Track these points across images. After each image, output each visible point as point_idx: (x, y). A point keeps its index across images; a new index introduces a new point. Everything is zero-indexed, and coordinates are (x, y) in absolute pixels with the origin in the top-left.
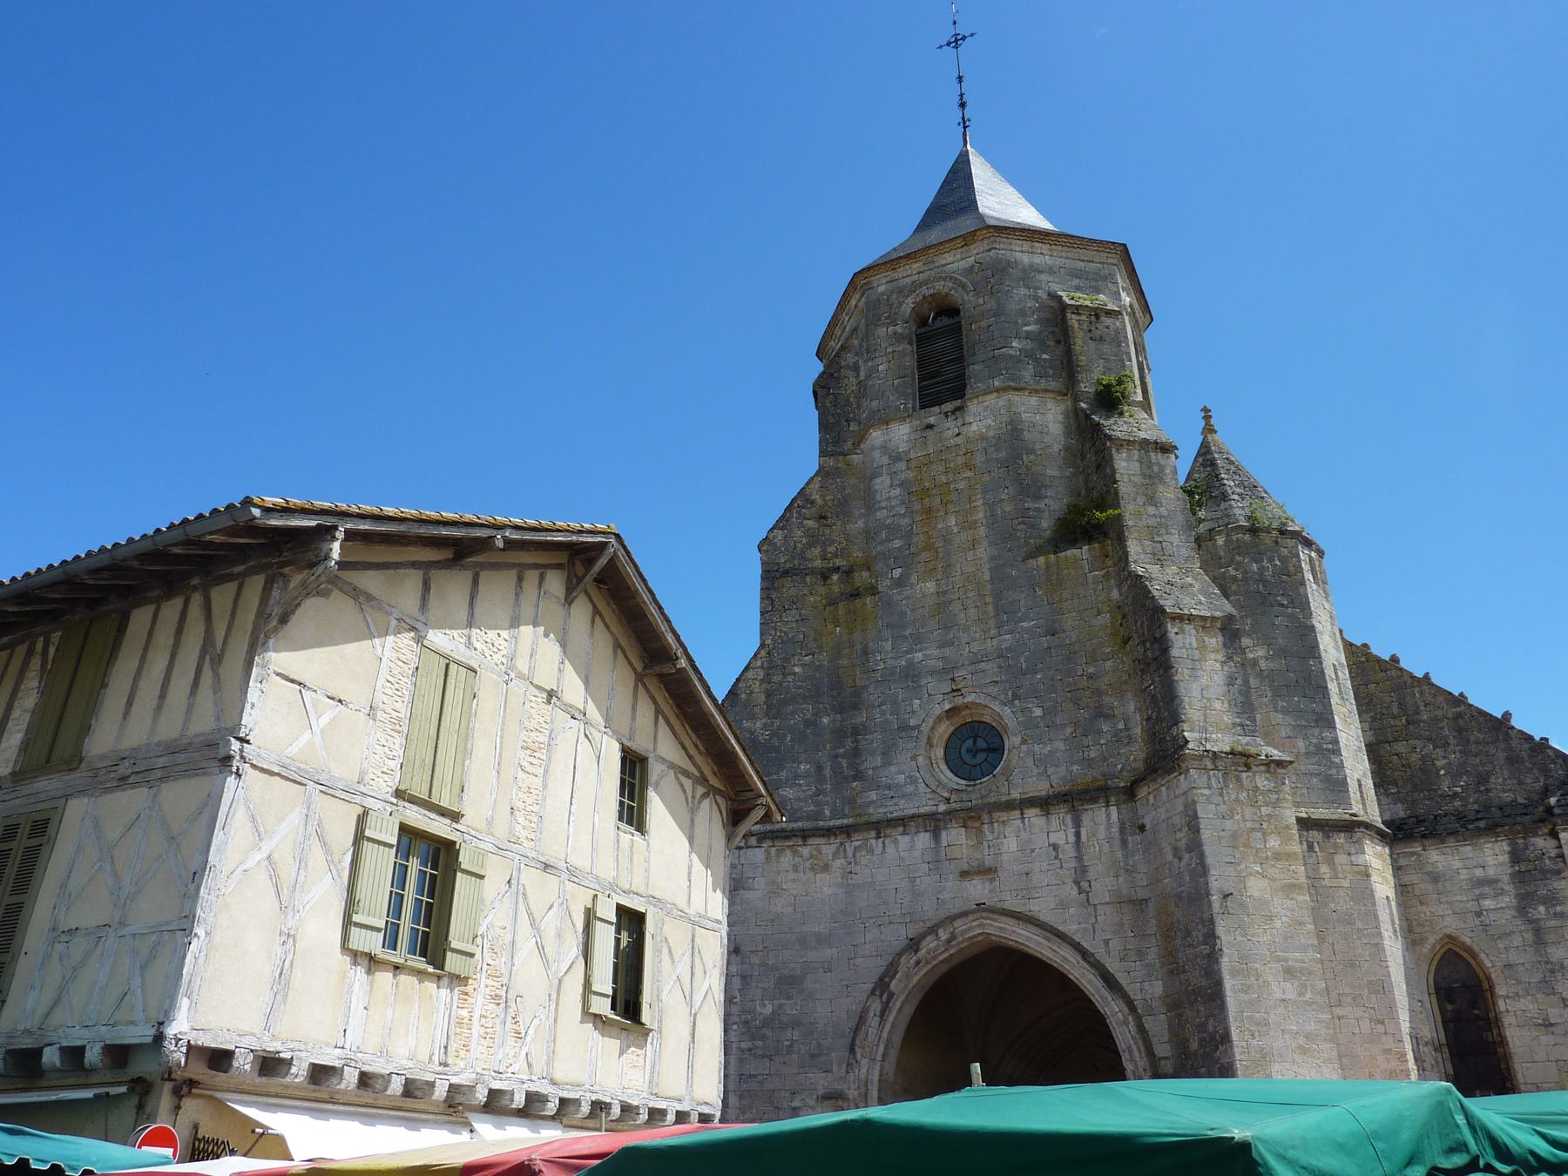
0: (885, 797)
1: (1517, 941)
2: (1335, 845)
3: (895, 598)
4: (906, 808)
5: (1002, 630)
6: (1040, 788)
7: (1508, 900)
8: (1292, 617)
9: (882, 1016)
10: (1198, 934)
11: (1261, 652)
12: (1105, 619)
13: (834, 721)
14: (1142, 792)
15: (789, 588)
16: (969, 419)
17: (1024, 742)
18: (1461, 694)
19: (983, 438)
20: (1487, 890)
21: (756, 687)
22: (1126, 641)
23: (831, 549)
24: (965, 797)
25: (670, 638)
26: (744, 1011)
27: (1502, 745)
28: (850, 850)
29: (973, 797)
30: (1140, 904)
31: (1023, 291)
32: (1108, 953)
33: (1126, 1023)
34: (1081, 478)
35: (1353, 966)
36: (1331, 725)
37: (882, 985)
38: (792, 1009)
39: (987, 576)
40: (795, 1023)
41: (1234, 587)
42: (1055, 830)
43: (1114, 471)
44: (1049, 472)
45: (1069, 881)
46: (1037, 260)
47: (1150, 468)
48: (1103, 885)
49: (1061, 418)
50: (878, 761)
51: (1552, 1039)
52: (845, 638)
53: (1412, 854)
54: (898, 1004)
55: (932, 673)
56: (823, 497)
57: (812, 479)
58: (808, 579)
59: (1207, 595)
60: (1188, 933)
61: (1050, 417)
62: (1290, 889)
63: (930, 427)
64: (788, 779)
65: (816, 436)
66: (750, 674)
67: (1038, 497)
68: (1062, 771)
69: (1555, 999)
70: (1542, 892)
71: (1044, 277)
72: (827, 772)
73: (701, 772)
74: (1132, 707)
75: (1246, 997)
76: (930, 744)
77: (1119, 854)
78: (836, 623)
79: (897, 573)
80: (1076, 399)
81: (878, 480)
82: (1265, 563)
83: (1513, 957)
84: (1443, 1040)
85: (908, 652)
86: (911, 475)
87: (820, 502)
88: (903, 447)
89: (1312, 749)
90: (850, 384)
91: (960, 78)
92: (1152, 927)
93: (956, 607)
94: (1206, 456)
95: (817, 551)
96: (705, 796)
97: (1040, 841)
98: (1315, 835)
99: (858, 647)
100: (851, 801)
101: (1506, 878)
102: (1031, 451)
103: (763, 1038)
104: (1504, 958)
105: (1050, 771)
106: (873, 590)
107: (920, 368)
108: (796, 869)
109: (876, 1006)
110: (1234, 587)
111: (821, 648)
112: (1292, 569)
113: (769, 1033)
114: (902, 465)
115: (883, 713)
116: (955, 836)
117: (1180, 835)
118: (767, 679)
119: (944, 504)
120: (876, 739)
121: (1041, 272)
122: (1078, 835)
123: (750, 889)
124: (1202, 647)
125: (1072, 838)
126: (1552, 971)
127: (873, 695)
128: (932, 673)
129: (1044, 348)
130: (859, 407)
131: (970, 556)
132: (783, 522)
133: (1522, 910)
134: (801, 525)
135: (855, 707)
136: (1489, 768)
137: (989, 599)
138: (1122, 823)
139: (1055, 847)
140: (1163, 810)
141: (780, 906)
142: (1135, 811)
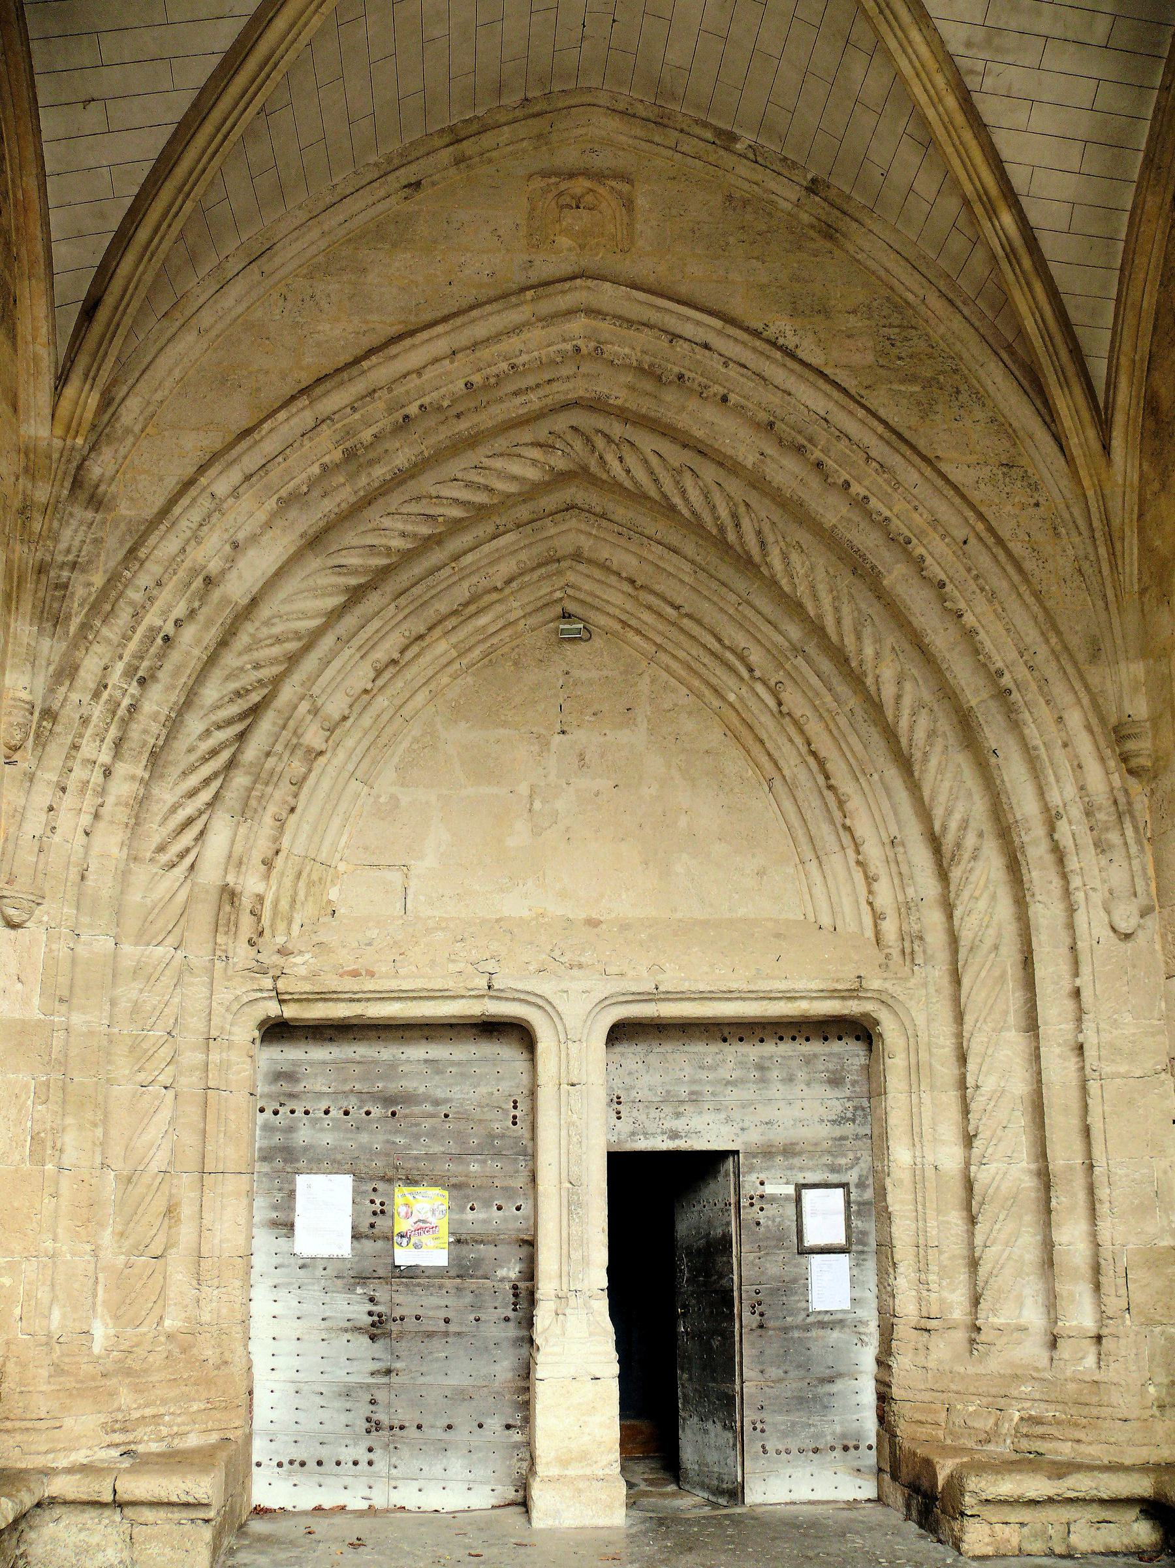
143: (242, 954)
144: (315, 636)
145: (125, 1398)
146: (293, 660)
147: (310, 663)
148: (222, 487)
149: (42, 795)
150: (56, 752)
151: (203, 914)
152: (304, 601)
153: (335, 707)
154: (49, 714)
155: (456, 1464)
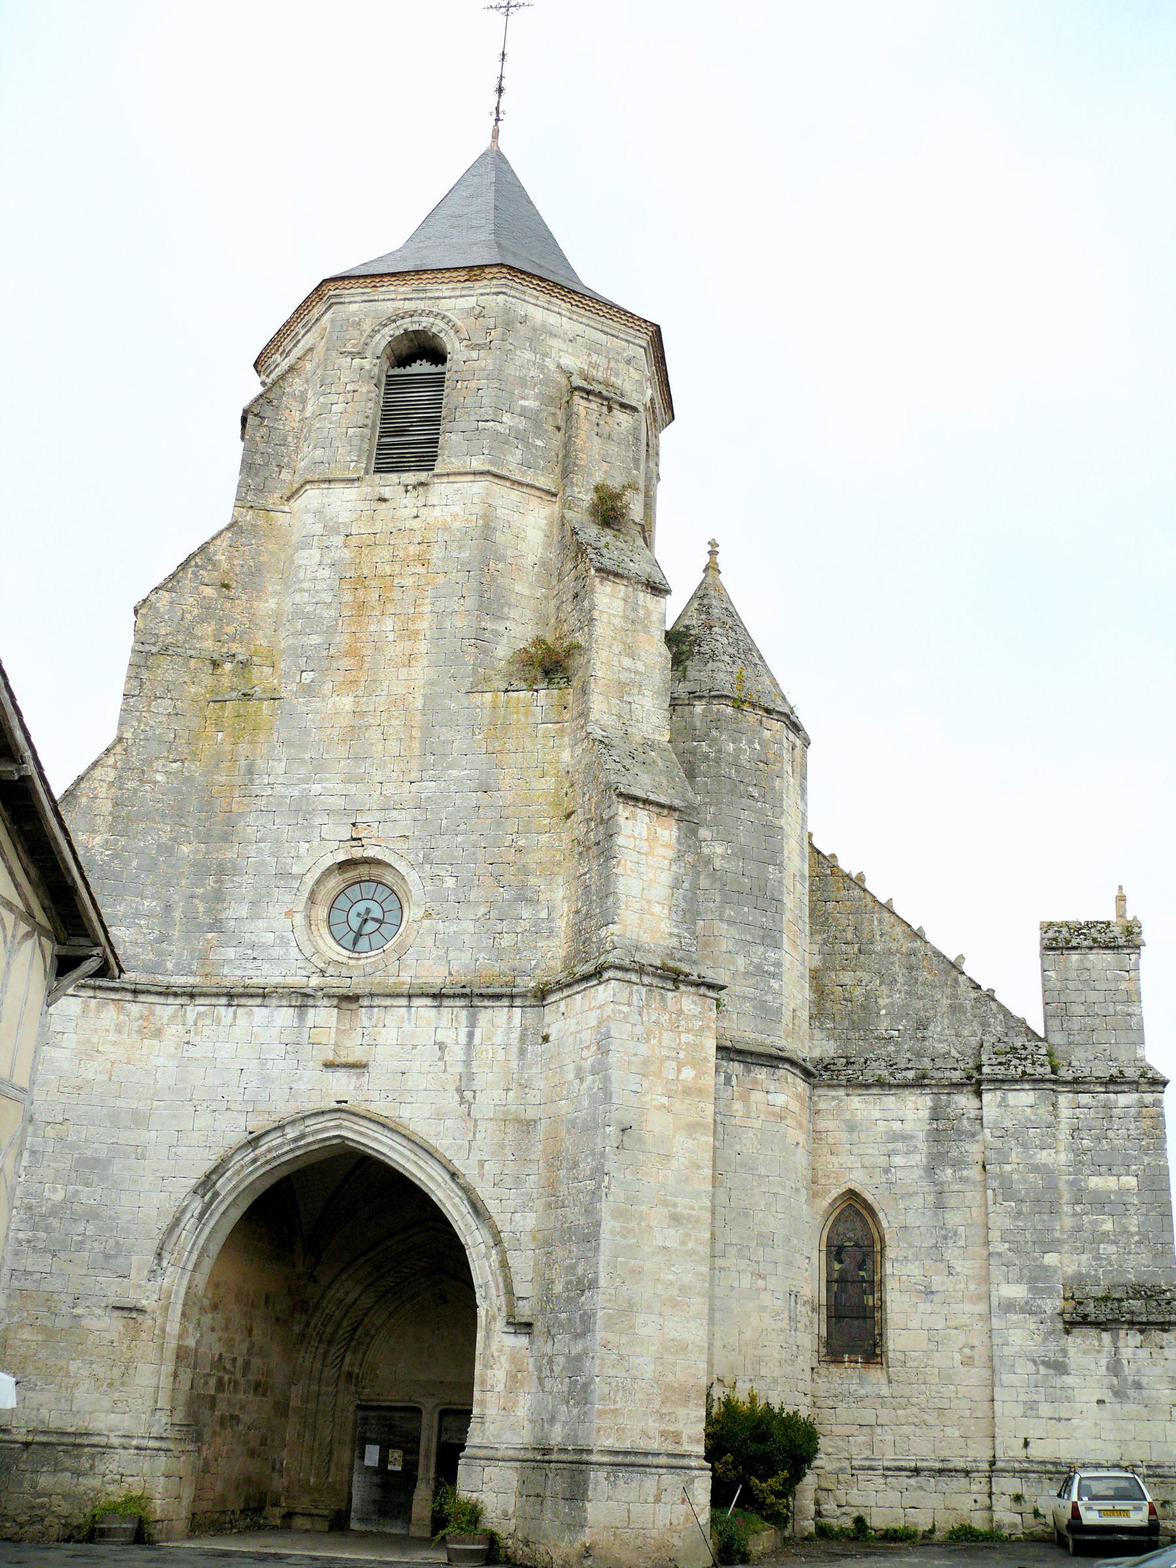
1: (919, 1201)
3: (301, 709)
4: (268, 975)
5: (426, 776)
6: (435, 975)
7: (920, 1159)
8: (762, 812)
10: (586, 1167)
11: (719, 850)
12: (549, 783)
13: (197, 851)
14: (551, 998)
15: (167, 671)
16: (432, 500)
17: (428, 915)
18: (920, 929)
19: (446, 528)
20: (900, 1145)
21: (103, 791)
23: (230, 629)
24: (345, 973)
25: (19, 734)
26: (28, 1194)
27: (949, 991)
29: (355, 973)
30: (528, 1125)
31: (528, 355)
32: (482, 1175)
34: (553, 603)
35: (746, 1215)
36: (777, 946)
37: (207, 1184)
38: (88, 1197)
39: (419, 703)
40: (91, 1216)
41: (703, 767)
42: (445, 1025)
43: (593, 607)
44: (518, 588)
45: (451, 1088)
47: (635, 610)
48: (490, 1097)
49: (543, 523)
50: (244, 911)
51: (928, 1307)
52: (228, 748)
53: (833, 1098)
54: (223, 1207)
55: (329, 812)
56: (230, 558)
58: (193, 662)
59: (670, 777)
60: (575, 1165)
61: (530, 519)
62: (693, 1128)
63: (382, 500)
64: (125, 916)
66: (98, 773)
67: (498, 617)
69: (942, 1266)
70: (954, 1154)
71: (556, 343)
72: (177, 914)
73: (28, 906)
74: (560, 894)
75: (623, 1242)
76: (312, 899)
77: (514, 1065)
78: (219, 726)
79: (308, 677)
80: (567, 505)
81: (305, 553)
82: (743, 745)
83: (911, 1220)
84: (824, 1301)
86: (347, 554)
87: (225, 565)
88: (344, 517)
89: (751, 969)
90: (291, 418)
91: (500, 90)
92: (537, 1151)
93: (374, 734)
94: (708, 596)
95: (209, 629)
96: (28, 935)
97: (425, 1037)
98: (736, 1068)
99: (242, 763)
100: (203, 958)
101: (922, 1135)
102: (501, 558)
104: (901, 1222)
105: (451, 955)
107: (385, 419)
108: (119, 1031)
109: (197, 1206)
110: (703, 767)
111: (194, 754)
112: (771, 757)
113: (54, 1222)
115: (260, 852)
116: (323, 1015)
117: (585, 1053)
119: (383, 601)
120: (243, 885)
122: (471, 1035)
123: (55, 1046)
124: (652, 839)
125: (463, 1039)
126: (945, 1238)
127: (251, 825)
128: (329, 812)
129: (539, 431)
130: (297, 450)
132: (171, 583)
133: (930, 1170)
135: (226, 838)
136: (931, 1013)
137: (416, 733)
138: (524, 1030)
139: (442, 1046)
140: (573, 1021)
141: (91, 1071)
142: (541, 1018)
143: (353, 1388)
144: (371, 1308)
145: (316, 1495)
146: (366, 1314)
147: (370, 1315)
148: (344, 1278)
149: (301, 1354)
150: (305, 1345)
151: (343, 1378)
152: (368, 1301)
153: (378, 1324)
154: (303, 1335)
155: (399, 1523)
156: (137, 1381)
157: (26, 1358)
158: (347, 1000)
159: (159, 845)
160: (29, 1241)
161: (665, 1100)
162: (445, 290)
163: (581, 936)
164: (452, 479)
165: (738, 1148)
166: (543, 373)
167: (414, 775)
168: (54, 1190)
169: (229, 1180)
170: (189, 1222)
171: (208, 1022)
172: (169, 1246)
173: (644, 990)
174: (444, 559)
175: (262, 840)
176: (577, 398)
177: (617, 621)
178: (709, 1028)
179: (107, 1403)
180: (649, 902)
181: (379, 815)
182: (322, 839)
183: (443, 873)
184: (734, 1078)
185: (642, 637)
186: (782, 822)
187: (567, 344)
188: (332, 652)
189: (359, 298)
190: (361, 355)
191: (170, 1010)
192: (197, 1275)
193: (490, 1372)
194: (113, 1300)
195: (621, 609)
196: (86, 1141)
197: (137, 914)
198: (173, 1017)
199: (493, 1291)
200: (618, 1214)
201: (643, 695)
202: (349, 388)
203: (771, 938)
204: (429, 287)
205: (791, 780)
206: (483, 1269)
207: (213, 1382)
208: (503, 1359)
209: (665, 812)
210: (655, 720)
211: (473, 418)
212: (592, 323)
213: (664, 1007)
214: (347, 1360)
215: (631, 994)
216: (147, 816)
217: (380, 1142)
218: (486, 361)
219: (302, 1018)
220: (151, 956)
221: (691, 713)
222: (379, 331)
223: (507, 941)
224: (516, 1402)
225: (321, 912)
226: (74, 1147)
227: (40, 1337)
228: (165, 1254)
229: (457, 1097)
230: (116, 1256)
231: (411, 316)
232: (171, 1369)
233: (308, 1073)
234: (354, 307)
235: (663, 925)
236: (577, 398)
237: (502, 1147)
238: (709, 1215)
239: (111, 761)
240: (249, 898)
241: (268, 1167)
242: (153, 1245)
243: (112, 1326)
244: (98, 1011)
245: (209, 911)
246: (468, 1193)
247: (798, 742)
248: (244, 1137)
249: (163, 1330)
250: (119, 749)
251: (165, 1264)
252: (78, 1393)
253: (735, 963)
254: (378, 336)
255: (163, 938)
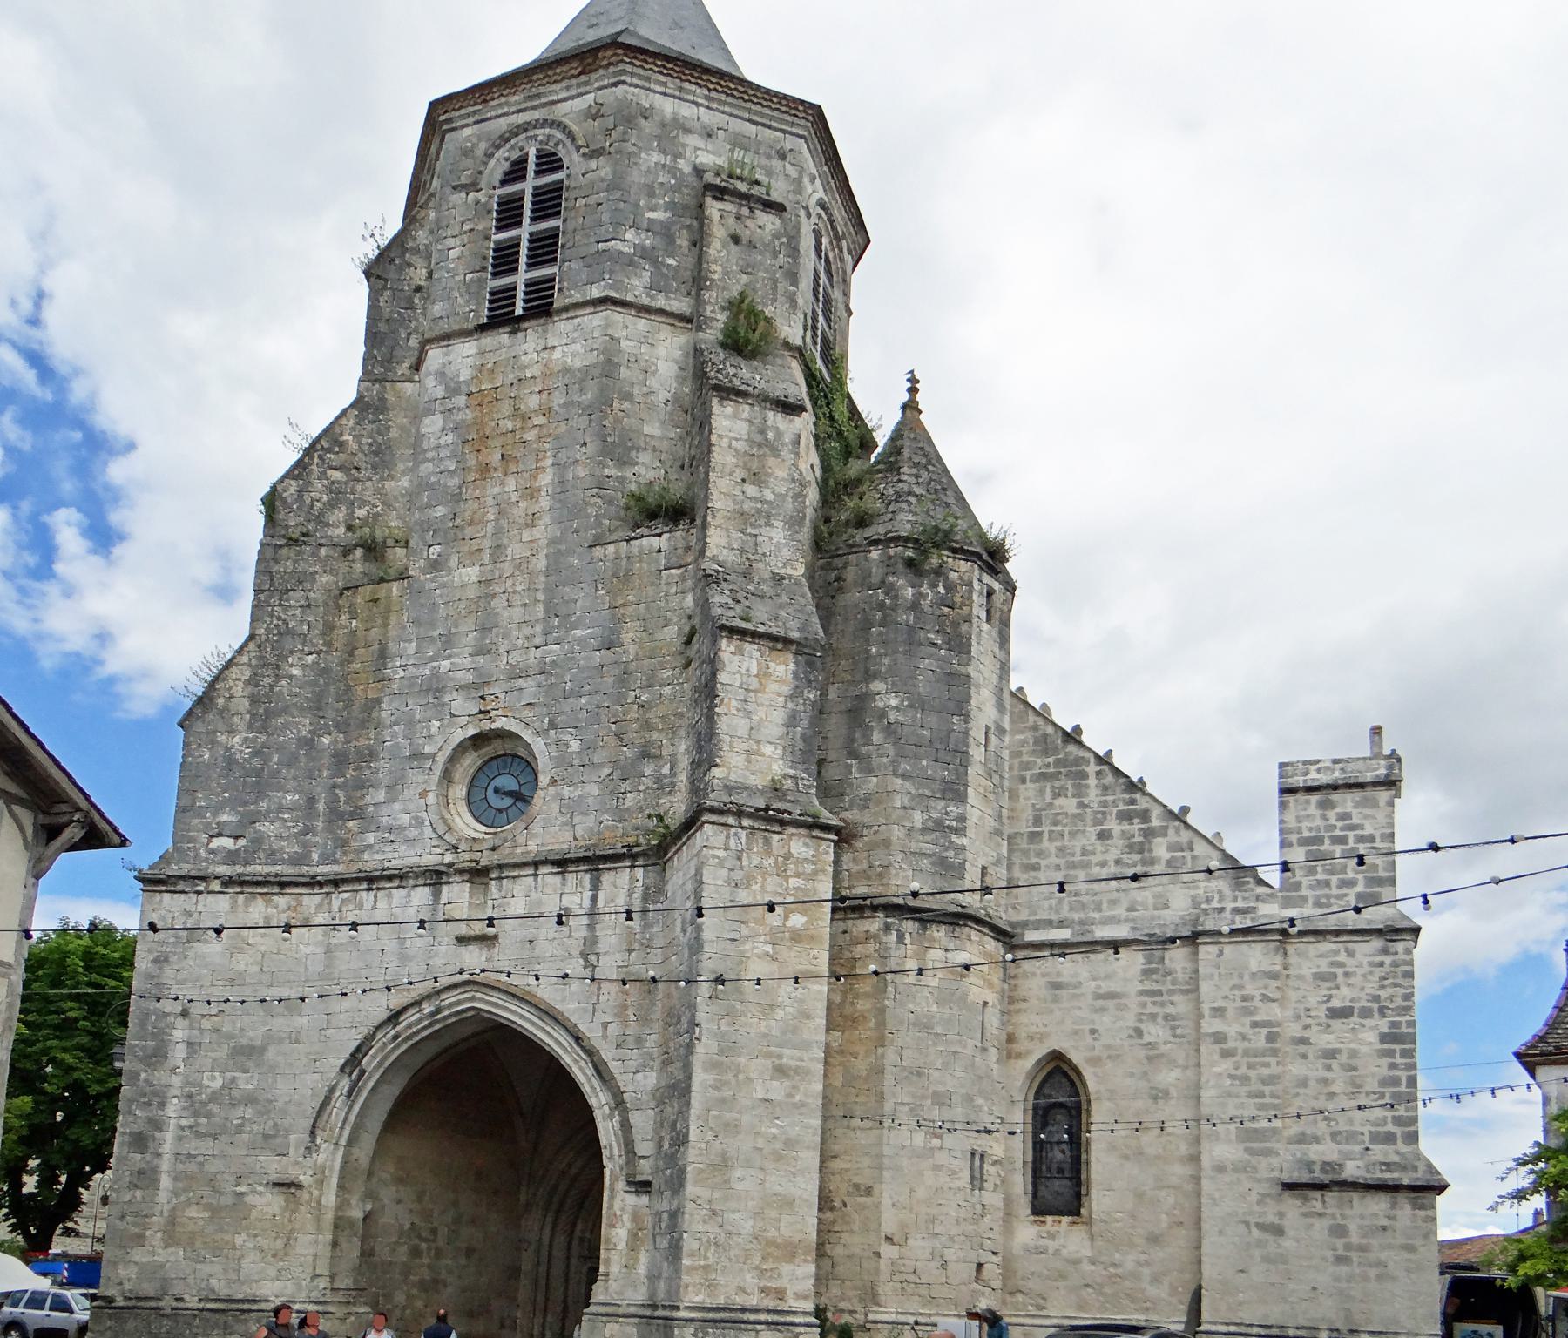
0: (382, 841)
2: (933, 940)
5: (550, 639)
9: (349, 1096)
19: (567, 370)
21: (239, 690)
22: (687, 665)
26: (187, 1083)
28: (336, 904)
31: (656, 157)
33: (611, 1117)
35: (919, 1074)
36: (961, 798)
37: (353, 1061)
40: (249, 1100)
42: (573, 891)
44: (647, 429)
45: (576, 953)
46: (687, 111)
49: (678, 353)
50: (381, 796)
54: (371, 1084)
57: (344, 412)
61: (662, 351)
64: (269, 811)
65: (362, 349)
68: (590, 821)
71: (692, 140)
72: (321, 806)
74: (683, 747)
76: (447, 777)
81: (427, 421)
82: (925, 589)
85: (432, 659)
86: (469, 415)
87: (353, 446)
89: (930, 824)
92: (658, 1013)
102: (627, 397)
103: (208, 1116)
105: (576, 820)
106: (403, 576)
109: (345, 1084)
111: (329, 644)
112: (958, 599)
113: (214, 1108)
114: (461, 400)
116: (457, 894)
118: (253, 681)
121: (688, 131)
122: (594, 899)
124: (764, 675)
125: (587, 903)
131: (526, 536)
134: (323, 475)
135: (363, 724)
137: (541, 596)
138: (647, 888)
156: (298, 1250)
157: (193, 1233)
158: (478, 875)
159: (299, 739)
160: (190, 1127)
161: (768, 948)
162: (558, 91)
163: (698, 788)
164: (571, 314)
165: (911, 1006)
166: (674, 177)
167: (538, 641)
168: (213, 1078)
169: (374, 1057)
170: (339, 1100)
171: (351, 907)
172: (320, 1124)
173: (743, 834)
174: (566, 405)
175: (396, 723)
176: (709, 201)
177: (741, 446)
178: (823, 871)
179: (272, 1272)
180: (759, 742)
181: (506, 686)
182: (453, 715)
183: (568, 737)
184: (907, 936)
185: (771, 461)
186: (971, 670)
187: (709, 140)
188: (458, 521)
189: (471, 120)
190: (473, 186)
191: (318, 899)
192: (356, 1152)
193: (614, 1232)
194: (273, 1177)
195: (744, 432)
196: (242, 1029)
197: (280, 809)
198: (319, 906)
199: (616, 1152)
200: (713, 1066)
201: (772, 526)
202: (466, 227)
203: (955, 791)
204: (542, 90)
205: (986, 627)
206: (607, 1131)
207: (404, 1249)
208: (626, 1218)
209: (780, 646)
210: (786, 553)
211: (592, 240)
212: (736, 112)
213: (768, 851)
214: (579, 1227)
215: (728, 837)
216: (285, 711)
217: (511, 1011)
218: (603, 169)
219: (437, 896)
220: (296, 849)
221: (866, 559)
222: (492, 155)
223: (630, 800)
224: (637, 1260)
225: (459, 791)
226: (230, 1037)
227: (207, 1215)
228: (318, 1132)
229: (581, 961)
230: (275, 1136)
231: (526, 130)
232: (329, 1237)
233: (443, 949)
234: (467, 132)
235: (775, 767)
236: (709, 201)
237: (625, 1007)
238: (821, 1066)
239: (245, 659)
240: (385, 782)
241: (410, 1043)
242: (308, 1124)
243: (269, 1203)
244: (246, 905)
245: (349, 800)
246: (591, 1053)
247: (996, 586)
248: (384, 1015)
249: (319, 1203)
250: (252, 646)
251: (318, 1141)
252: (245, 1263)
253: (910, 819)
254: (492, 162)
255: (307, 831)
